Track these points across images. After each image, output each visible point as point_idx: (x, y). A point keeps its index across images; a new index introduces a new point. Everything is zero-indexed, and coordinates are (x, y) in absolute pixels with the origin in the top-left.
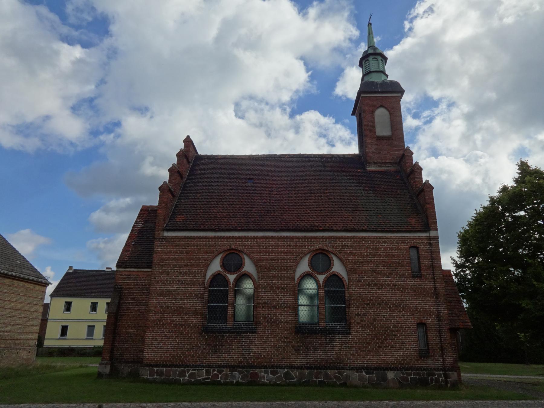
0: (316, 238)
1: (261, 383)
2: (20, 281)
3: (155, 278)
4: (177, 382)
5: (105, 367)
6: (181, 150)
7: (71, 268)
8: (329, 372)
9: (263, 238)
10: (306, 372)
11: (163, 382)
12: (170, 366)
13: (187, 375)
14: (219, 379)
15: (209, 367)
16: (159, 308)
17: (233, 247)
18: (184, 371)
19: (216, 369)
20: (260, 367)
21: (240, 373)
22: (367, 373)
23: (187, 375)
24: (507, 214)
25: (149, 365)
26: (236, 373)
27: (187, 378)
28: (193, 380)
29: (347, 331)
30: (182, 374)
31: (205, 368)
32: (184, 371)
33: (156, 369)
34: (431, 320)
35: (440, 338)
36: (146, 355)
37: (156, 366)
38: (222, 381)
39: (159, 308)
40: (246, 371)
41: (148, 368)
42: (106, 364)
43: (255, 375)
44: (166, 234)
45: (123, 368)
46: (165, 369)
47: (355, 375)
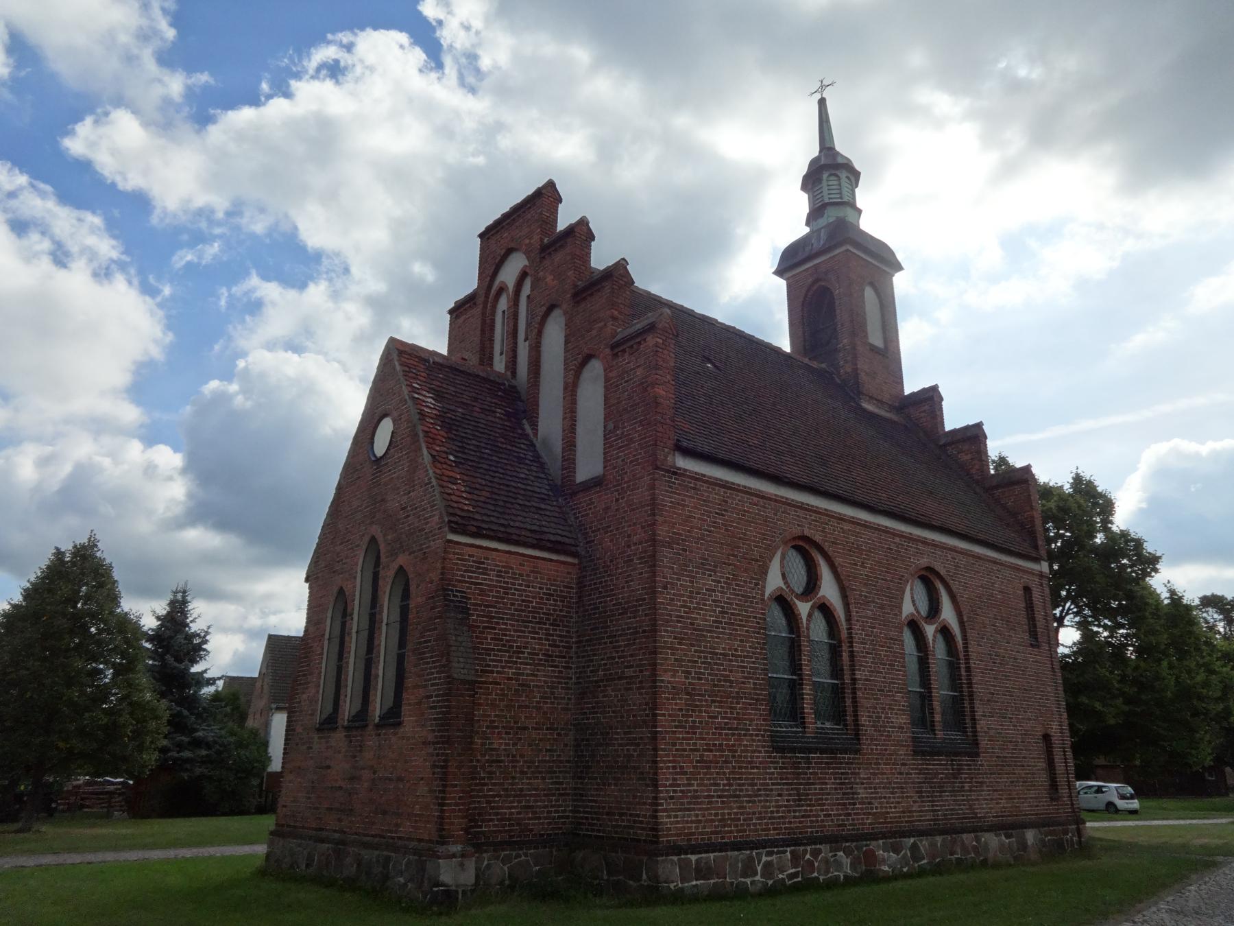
0: (925, 542)
1: (881, 874)
2: (483, 331)
3: (665, 587)
4: (741, 894)
5: (462, 865)
6: (633, 282)
7: (1009, 169)
8: (964, 836)
9: (854, 522)
10: (939, 839)
11: (716, 895)
12: (722, 847)
13: (759, 868)
14: (816, 874)
15: (796, 842)
16: (680, 677)
17: (807, 533)
18: (750, 858)
19: (809, 848)
20: (874, 837)
21: (848, 852)
22: (1007, 837)
23: (759, 868)
24: (1056, 567)
25: (678, 850)
26: (841, 853)
27: (758, 878)
28: (770, 882)
29: (973, 751)
30: (749, 870)
31: (788, 846)
32: (750, 858)
33: (693, 858)
34: (1054, 729)
35: (442, 811)
36: (665, 819)
37: (695, 849)
38: (821, 878)
39: (680, 677)
40: (857, 848)
41: (675, 858)
42: (463, 855)
43: (870, 857)
44: (682, 463)
45: (488, 866)
46: (712, 855)
47: (993, 841)
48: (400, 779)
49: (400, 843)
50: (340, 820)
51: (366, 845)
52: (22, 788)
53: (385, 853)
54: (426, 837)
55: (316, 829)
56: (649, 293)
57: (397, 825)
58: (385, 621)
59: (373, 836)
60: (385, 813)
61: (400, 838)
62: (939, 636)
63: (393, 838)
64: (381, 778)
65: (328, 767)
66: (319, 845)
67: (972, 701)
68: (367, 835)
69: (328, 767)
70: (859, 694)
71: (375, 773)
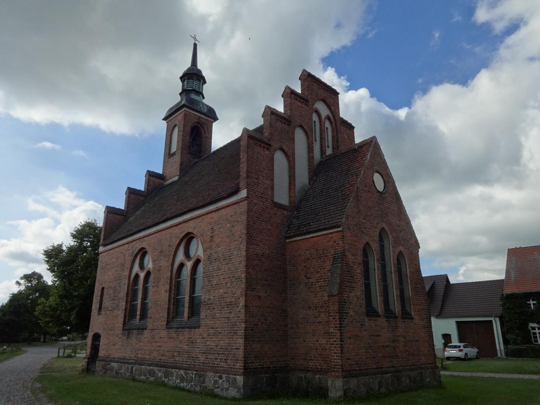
48: (417, 341)
49: (423, 366)
50: (391, 362)
51: (411, 370)
52: (437, 35)
53: (420, 371)
54: (430, 362)
55: (376, 368)
56: (410, 221)
57: (419, 360)
58: (393, 274)
59: (409, 366)
60: (413, 355)
61: (422, 364)
62: (409, 312)
63: (418, 365)
64: (408, 341)
65: (379, 336)
66: (384, 376)
67: (169, 308)
68: (407, 366)
69: (379, 336)
70: (167, 306)
71: (405, 338)
